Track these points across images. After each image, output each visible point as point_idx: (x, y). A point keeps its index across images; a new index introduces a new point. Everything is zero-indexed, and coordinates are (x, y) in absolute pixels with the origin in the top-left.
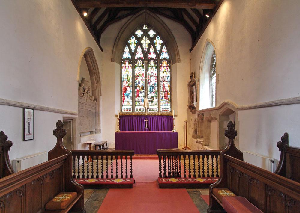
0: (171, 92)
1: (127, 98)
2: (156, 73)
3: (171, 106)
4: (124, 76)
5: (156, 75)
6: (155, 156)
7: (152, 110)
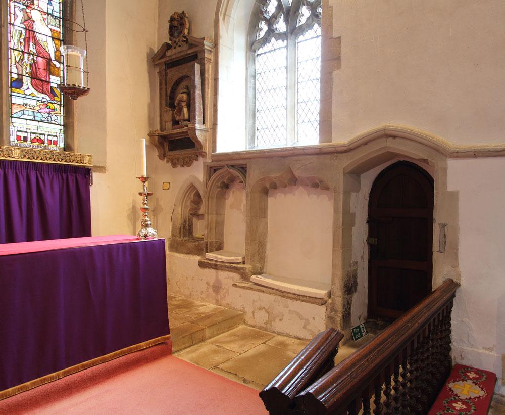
3: (68, 127)
6: (25, 389)
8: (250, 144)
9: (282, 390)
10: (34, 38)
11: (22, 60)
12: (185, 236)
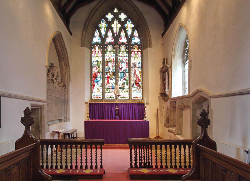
0: (142, 78)
2: (127, 58)
3: (142, 93)
4: (94, 62)
5: (127, 61)
7: (123, 98)
8: (184, 93)
9: (129, 138)
10: (136, 74)
11: (134, 80)
12: (167, 122)
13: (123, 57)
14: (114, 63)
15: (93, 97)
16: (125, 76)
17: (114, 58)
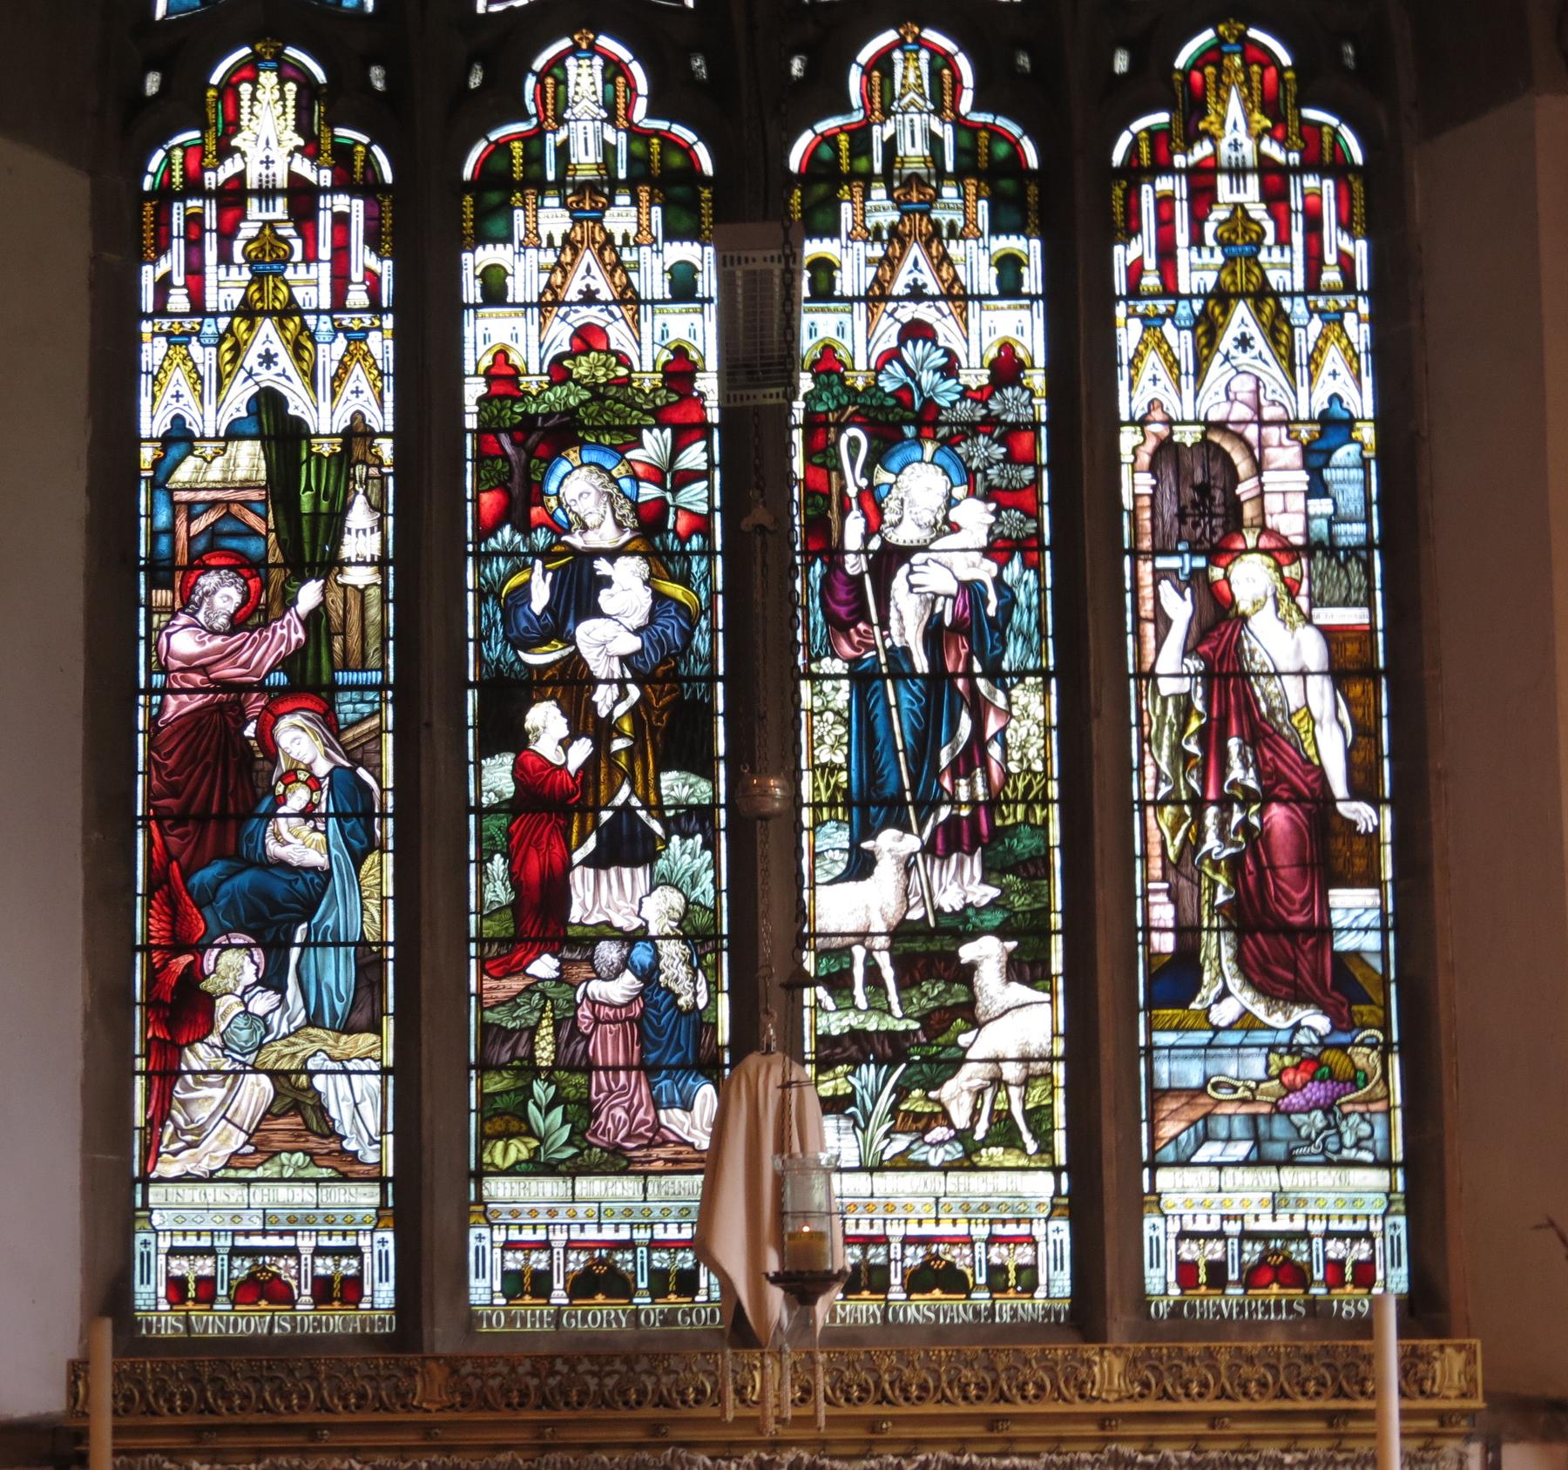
0: (1409, 806)
1: (272, 979)
2: (1024, 328)
4: (180, 438)
5: (1032, 398)
7: (918, 1281)
11: (1193, 845)
13: (909, 311)
14: (694, 457)
15: (149, 1294)
16: (973, 757)
17: (698, 330)
